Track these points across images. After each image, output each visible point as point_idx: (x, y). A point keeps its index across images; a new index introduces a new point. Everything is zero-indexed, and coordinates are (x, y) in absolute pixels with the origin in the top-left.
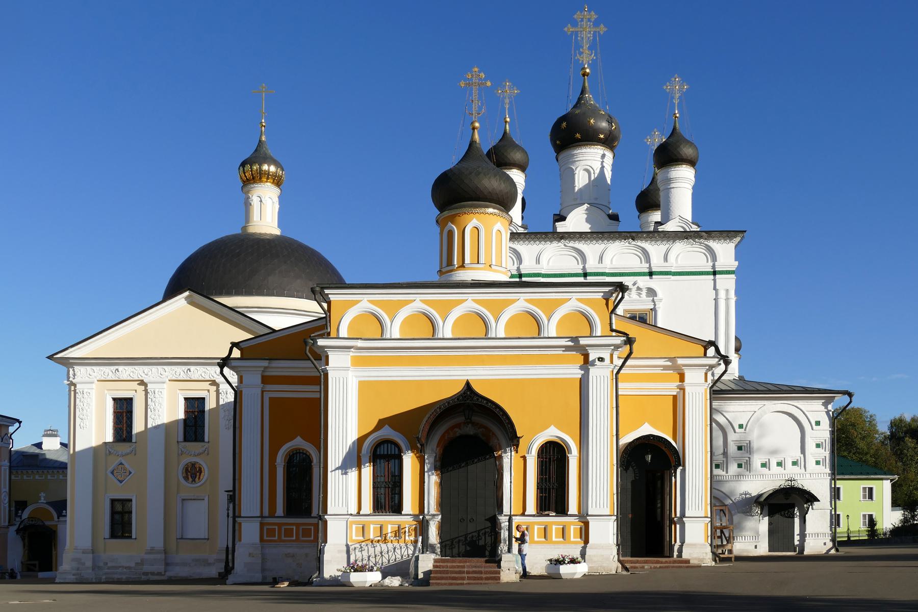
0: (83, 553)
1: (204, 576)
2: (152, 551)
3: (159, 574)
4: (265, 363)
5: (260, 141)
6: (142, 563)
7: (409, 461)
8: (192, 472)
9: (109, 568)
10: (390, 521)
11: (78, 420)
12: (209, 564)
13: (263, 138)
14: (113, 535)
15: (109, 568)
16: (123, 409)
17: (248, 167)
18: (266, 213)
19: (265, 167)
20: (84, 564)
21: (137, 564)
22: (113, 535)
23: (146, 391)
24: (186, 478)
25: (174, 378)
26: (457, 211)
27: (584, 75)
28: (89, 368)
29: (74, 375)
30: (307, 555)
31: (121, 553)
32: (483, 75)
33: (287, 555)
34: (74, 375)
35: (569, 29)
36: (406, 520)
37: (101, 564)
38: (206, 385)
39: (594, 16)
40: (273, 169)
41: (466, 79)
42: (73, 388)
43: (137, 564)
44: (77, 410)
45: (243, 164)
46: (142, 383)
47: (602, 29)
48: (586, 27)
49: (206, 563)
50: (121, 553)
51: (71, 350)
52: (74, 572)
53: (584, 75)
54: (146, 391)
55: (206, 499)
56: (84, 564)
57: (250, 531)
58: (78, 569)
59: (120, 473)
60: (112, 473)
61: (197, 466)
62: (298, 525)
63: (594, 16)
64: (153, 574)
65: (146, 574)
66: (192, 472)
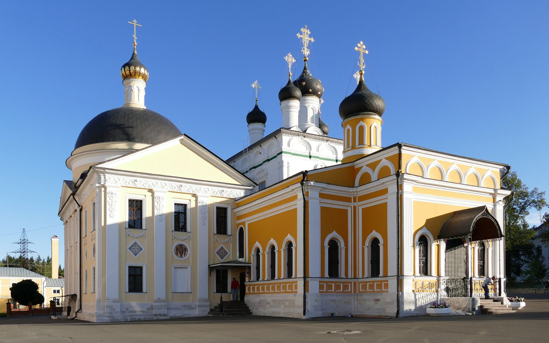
0: (114, 302)
1: (192, 316)
2: (159, 300)
3: (164, 315)
4: (325, 185)
5: (134, 54)
6: (152, 308)
7: (434, 246)
8: (181, 250)
9: (129, 312)
10: (427, 279)
11: (108, 213)
12: (192, 308)
13: (136, 53)
14: (131, 290)
15: (129, 312)
16: (136, 206)
17: (127, 68)
18: (138, 99)
19: (138, 69)
20: (114, 309)
21: (148, 309)
22: (131, 290)
23: (153, 196)
24: (177, 254)
25: (171, 190)
26: (364, 116)
27: (305, 61)
28: (116, 176)
29: (105, 181)
30: (340, 300)
31: (136, 303)
32: (364, 47)
33: (332, 300)
34: (105, 181)
35: (299, 35)
36: (433, 280)
37: (125, 310)
38: (190, 197)
39: (309, 33)
40: (143, 70)
41: (358, 47)
42: (103, 189)
43: (148, 309)
44: (107, 205)
45: (124, 66)
46: (150, 191)
47: (312, 40)
48: (305, 36)
49: (191, 308)
50: (136, 303)
51: (107, 163)
52: (108, 315)
53: (305, 61)
54: (153, 196)
55: (189, 268)
56: (114, 309)
57: (314, 286)
58: (111, 313)
59: (135, 249)
60: (130, 249)
61: (183, 247)
62: (335, 282)
63: (309, 33)
64: (160, 315)
65: (156, 315)
66: (181, 250)
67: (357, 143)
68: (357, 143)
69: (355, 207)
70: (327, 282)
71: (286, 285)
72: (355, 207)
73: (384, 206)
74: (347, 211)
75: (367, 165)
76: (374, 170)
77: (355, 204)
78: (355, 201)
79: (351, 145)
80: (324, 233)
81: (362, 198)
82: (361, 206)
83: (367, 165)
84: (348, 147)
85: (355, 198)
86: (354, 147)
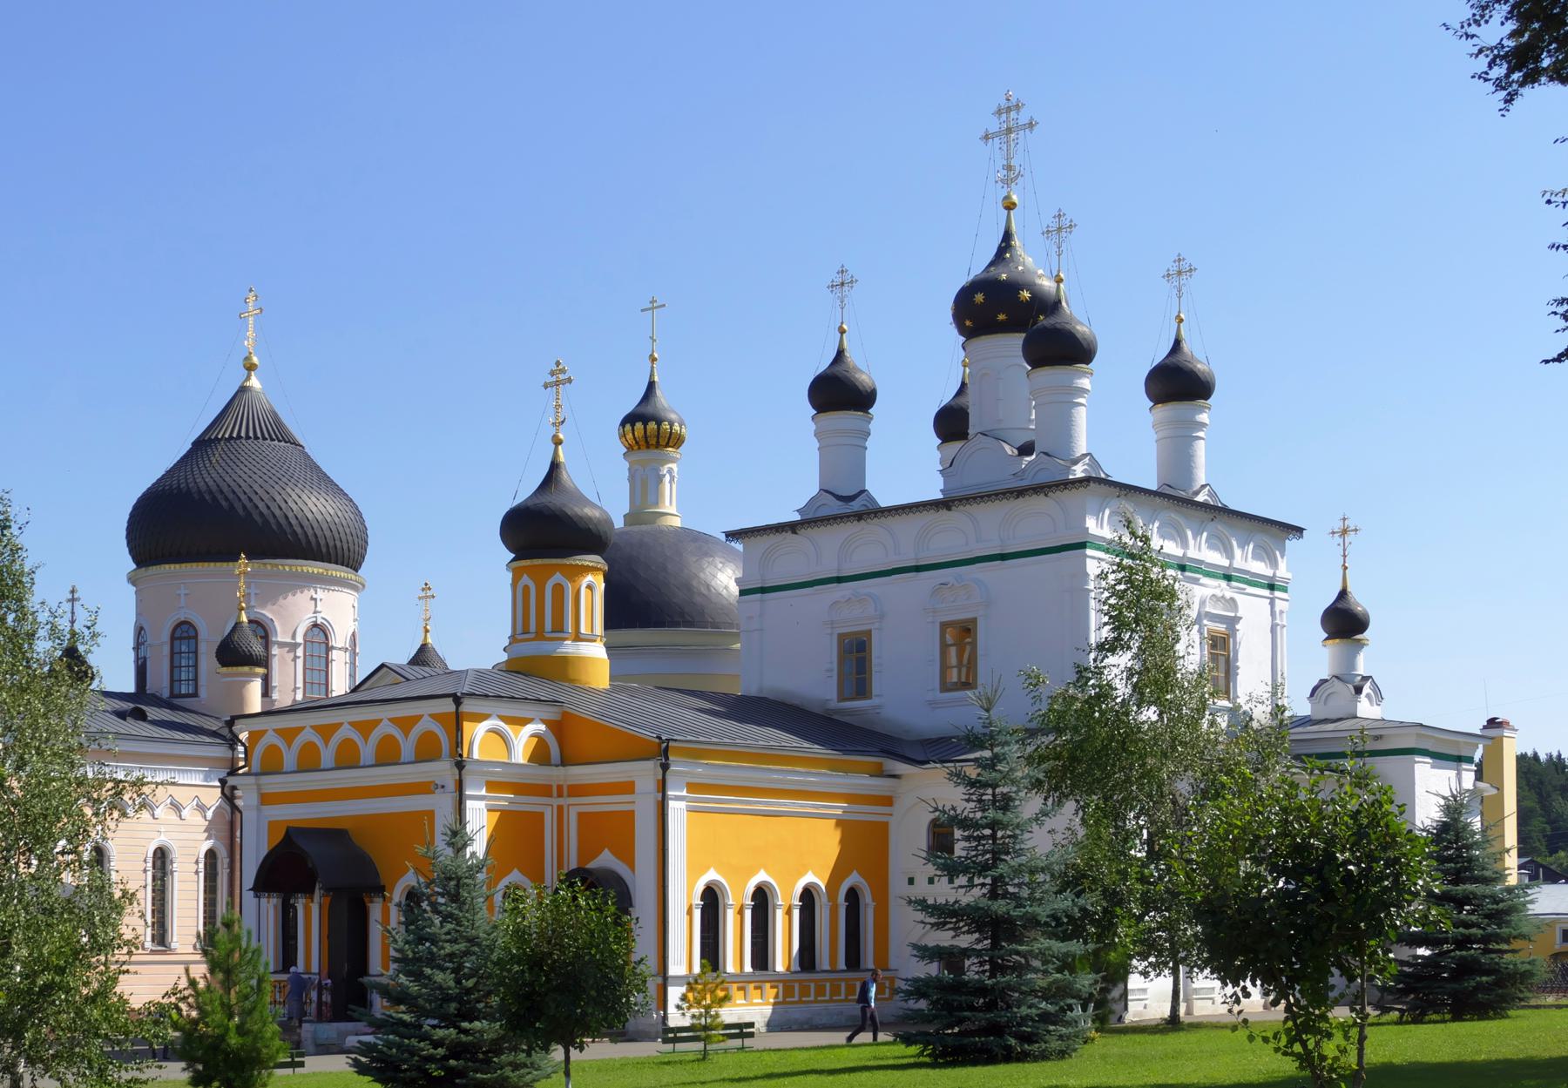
67: (548, 626)
68: (548, 626)
69: (560, 808)
70: (800, 981)
71: (801, 995)
72: (560, 808)
73: (629, 816)
74: (542, 814)
75: (391, 720)
76: (406, 732)
77: (561, 801)
78: (560, 795)
79: (533, 627)
80: (695, 870)
81: (577, 790)
82: (576, 807)
83: (391, 720)
84: (526, 632)
85: (560, 788)
86: (540, 635)
